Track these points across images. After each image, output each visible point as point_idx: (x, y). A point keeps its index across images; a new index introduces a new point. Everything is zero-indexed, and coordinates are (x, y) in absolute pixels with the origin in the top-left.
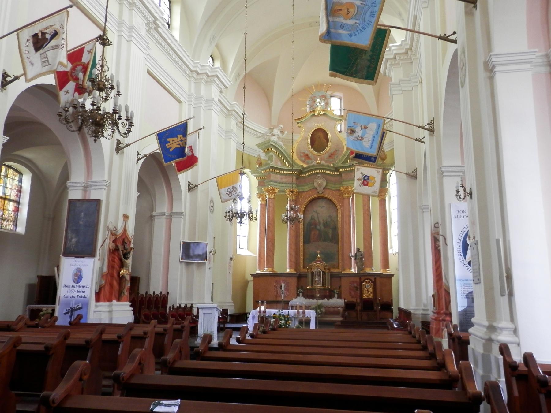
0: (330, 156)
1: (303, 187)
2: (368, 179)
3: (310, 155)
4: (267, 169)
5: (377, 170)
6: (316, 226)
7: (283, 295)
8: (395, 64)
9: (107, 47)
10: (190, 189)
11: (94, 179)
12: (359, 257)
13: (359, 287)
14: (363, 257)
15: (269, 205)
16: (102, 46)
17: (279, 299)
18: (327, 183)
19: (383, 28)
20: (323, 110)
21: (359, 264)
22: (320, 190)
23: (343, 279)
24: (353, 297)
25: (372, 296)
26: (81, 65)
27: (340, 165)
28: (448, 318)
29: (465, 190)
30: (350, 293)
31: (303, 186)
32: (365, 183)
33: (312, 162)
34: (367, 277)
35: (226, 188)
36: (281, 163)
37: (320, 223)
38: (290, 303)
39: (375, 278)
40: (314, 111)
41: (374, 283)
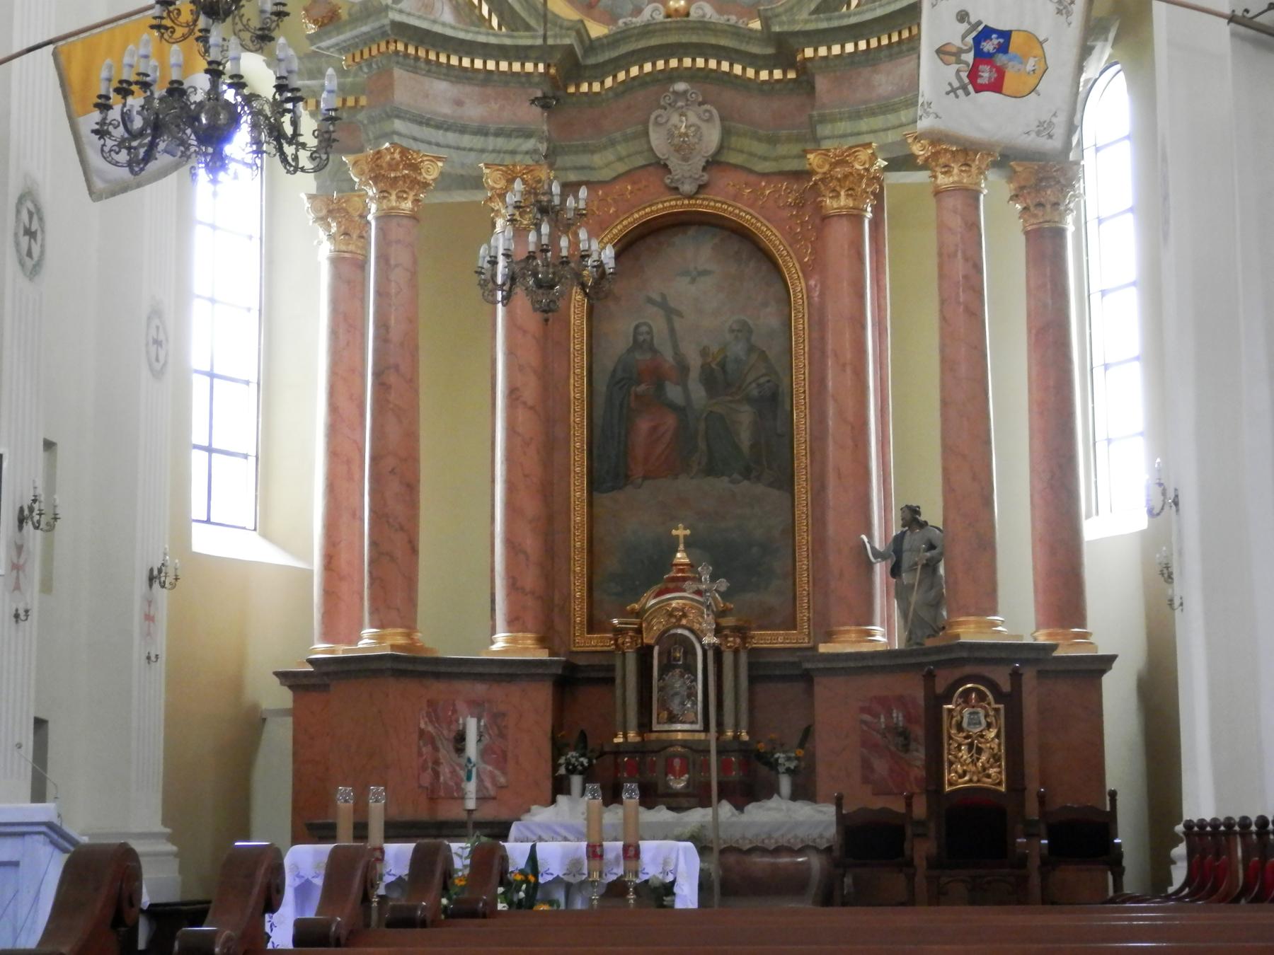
1: (584, 159)
2: (1003, 48)
4: (369, 39)
6: (660, 387)
12: (914, 554)
14: (937, 560)
15: (383, 258)
17: (449, 812)
18: (726, 132)
21: (914, 598)
22: (686, 172)
23: (823, 688)
25: (996, 777)
29: (1164, 493)
30: (866, 766)
32: (986, 75)
34: (968, 670)
37: (683, 369)
41: (1011, 701)
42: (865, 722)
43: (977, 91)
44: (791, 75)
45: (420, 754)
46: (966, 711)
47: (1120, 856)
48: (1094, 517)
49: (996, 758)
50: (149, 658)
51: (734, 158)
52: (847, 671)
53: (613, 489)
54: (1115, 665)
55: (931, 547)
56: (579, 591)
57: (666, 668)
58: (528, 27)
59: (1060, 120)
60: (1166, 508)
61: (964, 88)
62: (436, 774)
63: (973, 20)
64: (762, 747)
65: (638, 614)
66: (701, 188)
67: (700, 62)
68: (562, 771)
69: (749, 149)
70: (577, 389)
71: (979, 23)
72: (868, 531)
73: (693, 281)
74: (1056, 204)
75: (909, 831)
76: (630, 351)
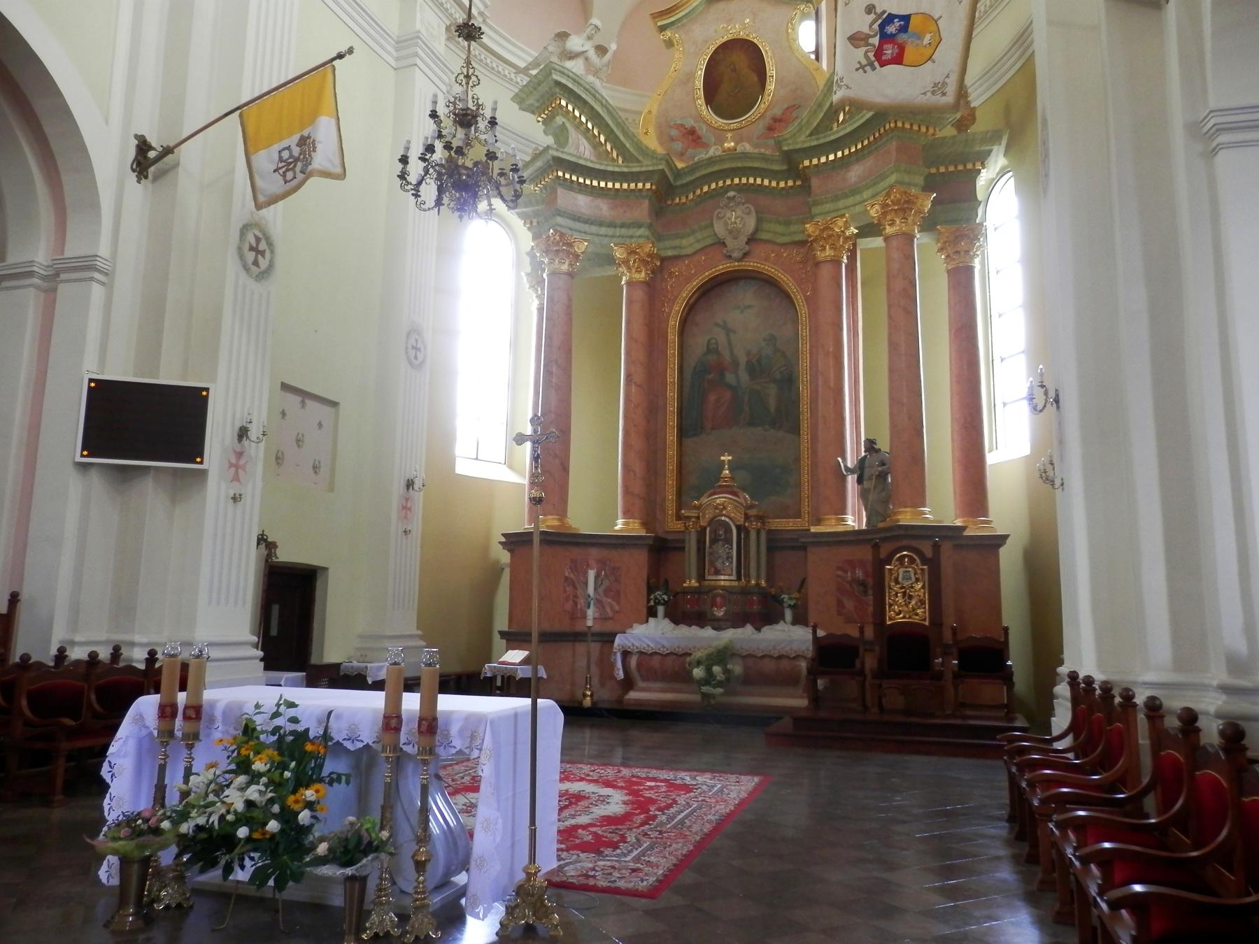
0: (770, 129)
1: (677, 242)
2: (904, 30)
3: (703, 130)
7: (591, 613)
12: (873, 470)
13: (870, 581)
14: (891, 472)
17: (579, 628)
18: (759, 221)
21: (872, 497)
22: (736, 246)
24: (849, 621)
25: (922, 615)
27: (803, 141)
29: (1046, 393)
30: (840, 604)
31: (677, 236)
32: (889, 51)
34: (904, 543)
35: (276, 147)
37: (736, 364)
38: (619, 640)
39: (934, 545)
41: (934, 565)
42: (838, 576)
43: (882, 66)
45: (565, 591)
46: (901, 570)
47: (1012, 674)
48: (995, 452)
49: (922, 602)
51: (764, 236)
52: (828, 544)
53: (695, 435)
54: (1008, 541)
55: (883, 464)
56: (671, 495)
57: (714, 541)
58: (638, 161)
59: (954, 78)
60: (1048, 405)
61: (871, 64)
62: (576, 604)
63: (879, 10)
64: (773, 591)
65: (698, 508)
66: (746, 255)
68: (652, 603)
69: (773, 230)
70: (672, 376)
71: (884, 12)
72: (843, 454)
73: (742, 312)
74: (967, 252)
75: (861, 650)
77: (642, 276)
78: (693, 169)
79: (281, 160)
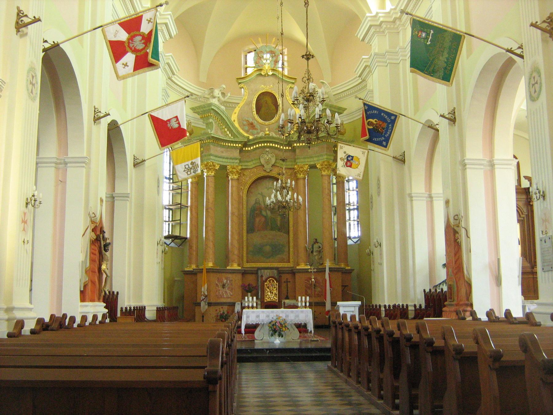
1: (246, 164)
2: (352, 159)
3: (255, 123)
5: (362, 150)
8: (379, 32)
9: (311, 60)
10: (135, 165)
11: (70, 155)
16: (306, 61)
18: (276, 159)
19: (458, 33)
20: (273, 70)
22: (268, 167)
23: (297, 276)
26: (140, 35)
28: (469, 309)
29: (539, 192)
32: (349, 164)
33: (258, 133)
36: (222, 133)
40: (261, 70)
44: (290, 148)
50: (24, 242)
51: (278, 165)
58: (237, 137)
67: (271, 145)
76: (255, 204)
77: (236, 177)
78: (254, 140)
79: (185, 168)
